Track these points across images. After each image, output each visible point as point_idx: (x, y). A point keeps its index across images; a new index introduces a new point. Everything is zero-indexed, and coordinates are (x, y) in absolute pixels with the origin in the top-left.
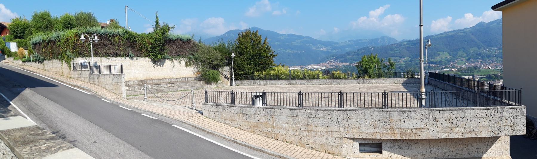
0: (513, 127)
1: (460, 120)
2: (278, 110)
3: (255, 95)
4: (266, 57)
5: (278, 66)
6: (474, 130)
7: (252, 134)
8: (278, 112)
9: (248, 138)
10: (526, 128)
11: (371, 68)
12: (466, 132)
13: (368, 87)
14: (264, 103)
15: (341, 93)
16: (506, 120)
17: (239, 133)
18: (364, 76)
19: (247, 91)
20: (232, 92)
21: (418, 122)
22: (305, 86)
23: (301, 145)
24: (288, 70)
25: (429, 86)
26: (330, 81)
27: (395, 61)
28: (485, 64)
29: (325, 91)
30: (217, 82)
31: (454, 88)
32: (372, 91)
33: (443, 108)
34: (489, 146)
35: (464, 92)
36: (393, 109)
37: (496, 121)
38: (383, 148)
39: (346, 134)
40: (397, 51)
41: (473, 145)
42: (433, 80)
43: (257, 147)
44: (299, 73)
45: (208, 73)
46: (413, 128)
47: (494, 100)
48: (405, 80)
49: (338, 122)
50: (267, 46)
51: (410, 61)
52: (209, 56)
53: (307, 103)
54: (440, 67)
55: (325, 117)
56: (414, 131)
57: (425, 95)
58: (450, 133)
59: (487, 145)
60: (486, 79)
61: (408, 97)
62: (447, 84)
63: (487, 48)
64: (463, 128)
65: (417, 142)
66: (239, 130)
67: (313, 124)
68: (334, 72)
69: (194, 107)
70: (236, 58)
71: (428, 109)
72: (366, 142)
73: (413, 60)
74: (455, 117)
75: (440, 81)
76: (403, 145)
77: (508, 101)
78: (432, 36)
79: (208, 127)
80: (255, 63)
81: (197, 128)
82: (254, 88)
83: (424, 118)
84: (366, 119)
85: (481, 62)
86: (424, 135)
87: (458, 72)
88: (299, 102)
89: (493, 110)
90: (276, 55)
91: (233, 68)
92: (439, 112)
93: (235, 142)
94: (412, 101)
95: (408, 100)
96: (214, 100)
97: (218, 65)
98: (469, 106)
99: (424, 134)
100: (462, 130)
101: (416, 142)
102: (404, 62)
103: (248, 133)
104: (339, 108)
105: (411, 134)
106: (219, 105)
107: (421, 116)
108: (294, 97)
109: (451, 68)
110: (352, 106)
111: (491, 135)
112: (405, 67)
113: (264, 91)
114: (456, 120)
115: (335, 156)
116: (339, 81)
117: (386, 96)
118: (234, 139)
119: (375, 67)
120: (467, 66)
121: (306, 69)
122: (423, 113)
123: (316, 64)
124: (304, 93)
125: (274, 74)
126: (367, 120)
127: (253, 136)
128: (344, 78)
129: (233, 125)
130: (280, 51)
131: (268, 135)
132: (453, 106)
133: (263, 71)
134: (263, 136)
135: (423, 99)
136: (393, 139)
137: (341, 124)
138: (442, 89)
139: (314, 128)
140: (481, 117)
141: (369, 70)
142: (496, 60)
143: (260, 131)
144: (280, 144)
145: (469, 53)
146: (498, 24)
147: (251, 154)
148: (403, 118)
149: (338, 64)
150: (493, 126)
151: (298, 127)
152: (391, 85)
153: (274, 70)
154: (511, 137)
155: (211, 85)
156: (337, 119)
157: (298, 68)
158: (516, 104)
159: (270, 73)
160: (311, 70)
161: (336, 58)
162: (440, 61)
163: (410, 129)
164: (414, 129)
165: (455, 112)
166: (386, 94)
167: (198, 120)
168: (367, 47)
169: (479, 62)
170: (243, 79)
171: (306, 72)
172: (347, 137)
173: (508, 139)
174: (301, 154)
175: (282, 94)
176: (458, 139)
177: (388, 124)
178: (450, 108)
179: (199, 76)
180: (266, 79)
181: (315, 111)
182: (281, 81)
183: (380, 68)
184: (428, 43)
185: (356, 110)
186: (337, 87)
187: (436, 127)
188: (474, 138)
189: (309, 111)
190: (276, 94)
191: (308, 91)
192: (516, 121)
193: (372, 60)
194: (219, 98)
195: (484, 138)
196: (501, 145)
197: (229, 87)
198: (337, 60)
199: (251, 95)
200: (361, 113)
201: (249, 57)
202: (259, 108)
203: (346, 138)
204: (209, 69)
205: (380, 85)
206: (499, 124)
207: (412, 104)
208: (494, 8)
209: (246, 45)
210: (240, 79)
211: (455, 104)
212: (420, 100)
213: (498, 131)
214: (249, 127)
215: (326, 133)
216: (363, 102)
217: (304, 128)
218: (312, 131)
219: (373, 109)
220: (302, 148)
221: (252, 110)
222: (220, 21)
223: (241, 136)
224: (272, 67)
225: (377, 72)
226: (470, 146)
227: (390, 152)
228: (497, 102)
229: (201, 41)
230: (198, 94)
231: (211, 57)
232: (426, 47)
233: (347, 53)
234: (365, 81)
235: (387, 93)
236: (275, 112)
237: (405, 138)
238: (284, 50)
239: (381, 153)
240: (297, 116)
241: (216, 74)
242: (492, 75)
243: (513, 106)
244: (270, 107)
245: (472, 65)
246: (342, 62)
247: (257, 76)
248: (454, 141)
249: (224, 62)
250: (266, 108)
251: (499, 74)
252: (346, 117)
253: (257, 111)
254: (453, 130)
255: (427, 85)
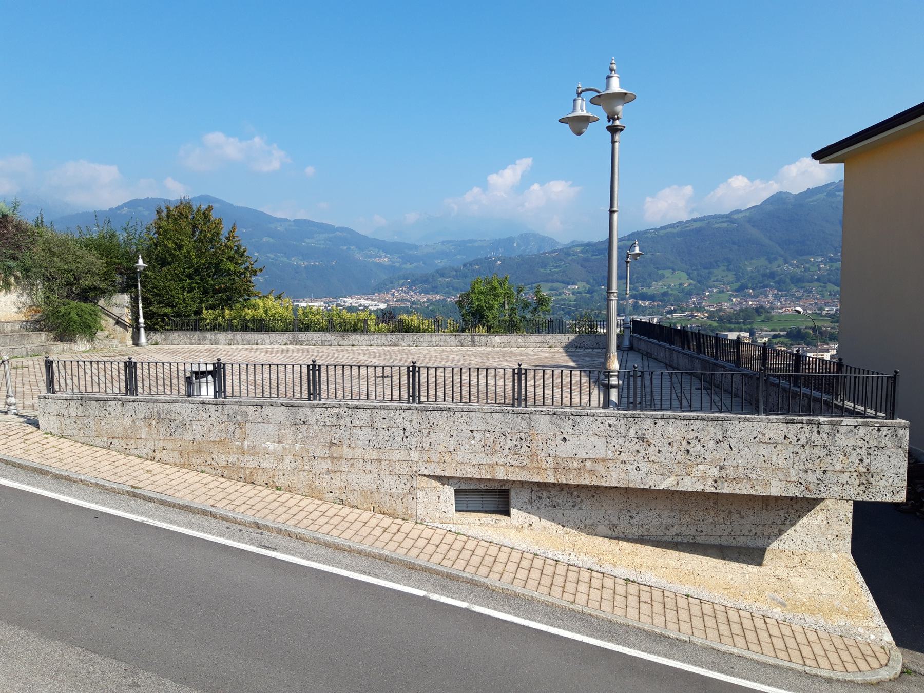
0: (866, 477)
1: (710, 446)
2: (254, 408)
3: (195, 369)
4: (235, 272)
5: (266, 297)
6: (749, 475)
7: (184, 470)
8: (256, 413)
9: (172, 483)
10: (905, 483)
11: (491, 308)
12: (725, 479)
13: (482, 354)
14: (220, 391)
15: (414, 367)
16: (845, 455)
17: (148, 472)
18: (474, 326)
19: (179, 359)
20: (130, 363)
21: (600, 443)
22: (332, 347)
23: (313, 493)
24: (290, 307)
25: (632, 356)
26: (394, 337)
27: (553, 292)
28: (786, 300)
29: (383, 363)
30: (92, 337)
31: (697, 364)
32: (493, 363)
33: (665, 413)
34: (788, 523)
35: (722, 374)
36: (537, 409)
37: (813, 456)
38: (512, 502)
39: (426, 465)
40: (557, 267)
41: (743, 513)
42: (643, 340)
43: (197, 503)
44: (317, 317)
45: (62, 309)
46: (587, 456)
47: (810, 399)
48: (572, 337)
49: (407, 437)
50: (235, 246)
51: (589, 292)
52: (67, 263)
53: (332, 391)
54: (664, 307)
55: (375, 425)
56: (588, 464)
57: (618, 378)
58: (681, 477)
59: (783, 518)
60: (786, 340)
61: (576, 379)
62: (679, 352)
63: (794, 258)
64: (718, 467)
65: (595, 491)
66: (149, 462)
67: (346, 442)
68: (404, 317)
69: (12, 407)
70: (150, 273)
71: (625, 412)
72: (472, 487)
73: (597, 291)
74: (697, 437)
75: (661, 343)
76: (562, 498)
77: (852, 405)
78: (646, 232)
79: (55, 460)
80: (204, 288)
81: (20, 466)
82: (200, 351)
83: (614, 434)
84: (472, 431)
85: (775, 296)
86: (615, 475)
87: (709, 322)
88: (311, 387)
89: (804, 425)
90: (261, 270)
91: (140, 299)
92: (652, 421)
93: (135, 495)
94: (585, 389)
95: (576, 387)
96: (82, 383)
97: (95, 288)
98: (736, 413)
99: (613, 474)
100: (716, 472)
101: (592, 493)
102: (573, 293)
103: (175, 469)
104: (409, 402)
105: (582, 471)
106: (91, 399)
107: (608, 428)
108: (297, 376)
109: (692, 310)
110: (440, 399)
111: (797, 492)
112: (575, 306)
113: (219, 360)
114: (698, 447)
115: (396, 521)
116: (415, 337)
117: (523, 376)
118: (132, 487)
119: (503, 305)
120: (736, 306)
121: (341, 306)
122: (612, 421)
123: (364, 294)
124: (330, 365)
125: (253, 316)
126: (475, 432)
127: (186, 477)
128: (429, 331)
129: (133, 451)
130: (273, 259)
131: (229, 472)
132: (691, 409)
133: (226, 309)
134: (215, 475)
135: (613, 386)
136: (537, 481)
137: (413, 441)
138: (667, 365)
139: (347, 452)
140: (769, 443)
141: (487, 313)
142: (820, 289)
143: (206, 464)
144: (260, 495)
145: (743, 274)
146: (831, 194)
147: (178, 525)
148: (562, 433)
149: (414, 296)
150: (802, 467)
151: (307, 449)
152: (540, 349)
153: (255, 307)
154: (857, 504)
155: (73, 345)
156: (404, 429)
157: (318, 304)
158: (879, 414)
159: (243, 314)
160: (351, 309)
161: (413, 282)
162: (665, 294)
163: (579, 459)
164: (589, 459)
165: (697, 424)
166: (523, 371)
167: (23, 445)
168: (486, 258)
169: (770, 295)
170: (169, 328)
171: (337, 314)
172: (427, 474)
173: (847, 510)
174: (313, 516)
175: (274, 368)
176: (702, 494)
177: (524, 444)
178: (682, 414)
179: (36, 317)
180: (233, 330)
181: (350, 411)
182: (273, 335)
183: (516, 309)
184: (634, 251)
185: (449, 410)
186: (411, 354)
187: (644, 458)
188: (748, 495)
189: (336, 410)
190: (258, 367)
191: (339, 361)
192: (876, 462)
193: (495, 290)
194: (95, 378)
195: (776, 498)
196: (825, 522)
197: (127, 348)
198: (414, 288)
199: (185, 371)
200: (462, 417)
201: (187, 271)
202: (204, 403)
203: (425, 476)
204: (66, 300)
205: (513, 349)
206: (821, 465)
207: (585, 400)
208: (819, 156)
209: (178, 239)
210: (161, 327)
211: (696, 402)
212: (606, 388)
213: (819, 484)
214: (176, 454)
215: (376, 465)
216: (466, 389)
217: (323, 451)
218: (341, 458)
219: (490, 407)
220: (317, 501)
221: (186, 411)
222: (108, 173)
223: (153, 479)
224: (248, 299)
225: (507, 318)
226: (735, 517)
227: (529, 513)
228: (818, 405)
229: (42, 222)
230: (31, 369)
231: (73, 266)
232: (629, 260)
233: (437, 271)
234: (477, 339)
235: (526, 370)
236: (249, 413)
237: (567, 479)
238: (285, 259)
239: (507, 513)
240: (304, 422)
241: (91, 314)
242: (806, 328)
243: (868, 420)
244: (235, 402)
245: (751, 303)
246: (427, 292)
247: (208, 321)
248: (693, 499)
249: (114, 281)
250: (223, 404)
251: (827, 326)
252: (424, 425)
253: (200, 411)
254: (690, 469)
255: (626, 353)
